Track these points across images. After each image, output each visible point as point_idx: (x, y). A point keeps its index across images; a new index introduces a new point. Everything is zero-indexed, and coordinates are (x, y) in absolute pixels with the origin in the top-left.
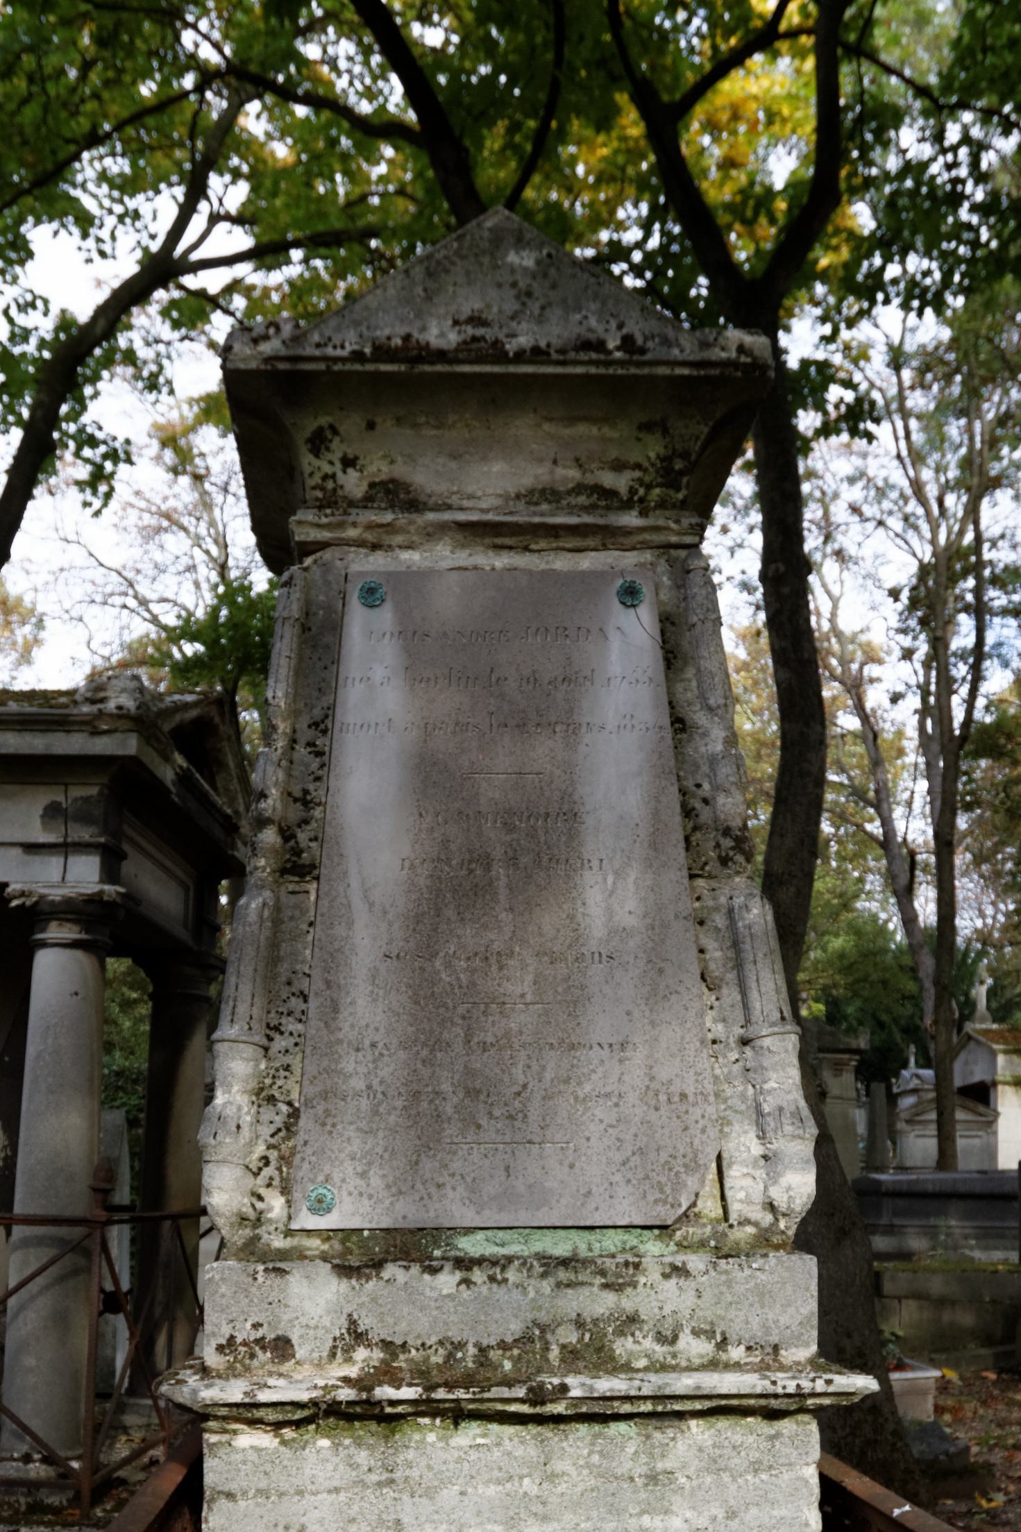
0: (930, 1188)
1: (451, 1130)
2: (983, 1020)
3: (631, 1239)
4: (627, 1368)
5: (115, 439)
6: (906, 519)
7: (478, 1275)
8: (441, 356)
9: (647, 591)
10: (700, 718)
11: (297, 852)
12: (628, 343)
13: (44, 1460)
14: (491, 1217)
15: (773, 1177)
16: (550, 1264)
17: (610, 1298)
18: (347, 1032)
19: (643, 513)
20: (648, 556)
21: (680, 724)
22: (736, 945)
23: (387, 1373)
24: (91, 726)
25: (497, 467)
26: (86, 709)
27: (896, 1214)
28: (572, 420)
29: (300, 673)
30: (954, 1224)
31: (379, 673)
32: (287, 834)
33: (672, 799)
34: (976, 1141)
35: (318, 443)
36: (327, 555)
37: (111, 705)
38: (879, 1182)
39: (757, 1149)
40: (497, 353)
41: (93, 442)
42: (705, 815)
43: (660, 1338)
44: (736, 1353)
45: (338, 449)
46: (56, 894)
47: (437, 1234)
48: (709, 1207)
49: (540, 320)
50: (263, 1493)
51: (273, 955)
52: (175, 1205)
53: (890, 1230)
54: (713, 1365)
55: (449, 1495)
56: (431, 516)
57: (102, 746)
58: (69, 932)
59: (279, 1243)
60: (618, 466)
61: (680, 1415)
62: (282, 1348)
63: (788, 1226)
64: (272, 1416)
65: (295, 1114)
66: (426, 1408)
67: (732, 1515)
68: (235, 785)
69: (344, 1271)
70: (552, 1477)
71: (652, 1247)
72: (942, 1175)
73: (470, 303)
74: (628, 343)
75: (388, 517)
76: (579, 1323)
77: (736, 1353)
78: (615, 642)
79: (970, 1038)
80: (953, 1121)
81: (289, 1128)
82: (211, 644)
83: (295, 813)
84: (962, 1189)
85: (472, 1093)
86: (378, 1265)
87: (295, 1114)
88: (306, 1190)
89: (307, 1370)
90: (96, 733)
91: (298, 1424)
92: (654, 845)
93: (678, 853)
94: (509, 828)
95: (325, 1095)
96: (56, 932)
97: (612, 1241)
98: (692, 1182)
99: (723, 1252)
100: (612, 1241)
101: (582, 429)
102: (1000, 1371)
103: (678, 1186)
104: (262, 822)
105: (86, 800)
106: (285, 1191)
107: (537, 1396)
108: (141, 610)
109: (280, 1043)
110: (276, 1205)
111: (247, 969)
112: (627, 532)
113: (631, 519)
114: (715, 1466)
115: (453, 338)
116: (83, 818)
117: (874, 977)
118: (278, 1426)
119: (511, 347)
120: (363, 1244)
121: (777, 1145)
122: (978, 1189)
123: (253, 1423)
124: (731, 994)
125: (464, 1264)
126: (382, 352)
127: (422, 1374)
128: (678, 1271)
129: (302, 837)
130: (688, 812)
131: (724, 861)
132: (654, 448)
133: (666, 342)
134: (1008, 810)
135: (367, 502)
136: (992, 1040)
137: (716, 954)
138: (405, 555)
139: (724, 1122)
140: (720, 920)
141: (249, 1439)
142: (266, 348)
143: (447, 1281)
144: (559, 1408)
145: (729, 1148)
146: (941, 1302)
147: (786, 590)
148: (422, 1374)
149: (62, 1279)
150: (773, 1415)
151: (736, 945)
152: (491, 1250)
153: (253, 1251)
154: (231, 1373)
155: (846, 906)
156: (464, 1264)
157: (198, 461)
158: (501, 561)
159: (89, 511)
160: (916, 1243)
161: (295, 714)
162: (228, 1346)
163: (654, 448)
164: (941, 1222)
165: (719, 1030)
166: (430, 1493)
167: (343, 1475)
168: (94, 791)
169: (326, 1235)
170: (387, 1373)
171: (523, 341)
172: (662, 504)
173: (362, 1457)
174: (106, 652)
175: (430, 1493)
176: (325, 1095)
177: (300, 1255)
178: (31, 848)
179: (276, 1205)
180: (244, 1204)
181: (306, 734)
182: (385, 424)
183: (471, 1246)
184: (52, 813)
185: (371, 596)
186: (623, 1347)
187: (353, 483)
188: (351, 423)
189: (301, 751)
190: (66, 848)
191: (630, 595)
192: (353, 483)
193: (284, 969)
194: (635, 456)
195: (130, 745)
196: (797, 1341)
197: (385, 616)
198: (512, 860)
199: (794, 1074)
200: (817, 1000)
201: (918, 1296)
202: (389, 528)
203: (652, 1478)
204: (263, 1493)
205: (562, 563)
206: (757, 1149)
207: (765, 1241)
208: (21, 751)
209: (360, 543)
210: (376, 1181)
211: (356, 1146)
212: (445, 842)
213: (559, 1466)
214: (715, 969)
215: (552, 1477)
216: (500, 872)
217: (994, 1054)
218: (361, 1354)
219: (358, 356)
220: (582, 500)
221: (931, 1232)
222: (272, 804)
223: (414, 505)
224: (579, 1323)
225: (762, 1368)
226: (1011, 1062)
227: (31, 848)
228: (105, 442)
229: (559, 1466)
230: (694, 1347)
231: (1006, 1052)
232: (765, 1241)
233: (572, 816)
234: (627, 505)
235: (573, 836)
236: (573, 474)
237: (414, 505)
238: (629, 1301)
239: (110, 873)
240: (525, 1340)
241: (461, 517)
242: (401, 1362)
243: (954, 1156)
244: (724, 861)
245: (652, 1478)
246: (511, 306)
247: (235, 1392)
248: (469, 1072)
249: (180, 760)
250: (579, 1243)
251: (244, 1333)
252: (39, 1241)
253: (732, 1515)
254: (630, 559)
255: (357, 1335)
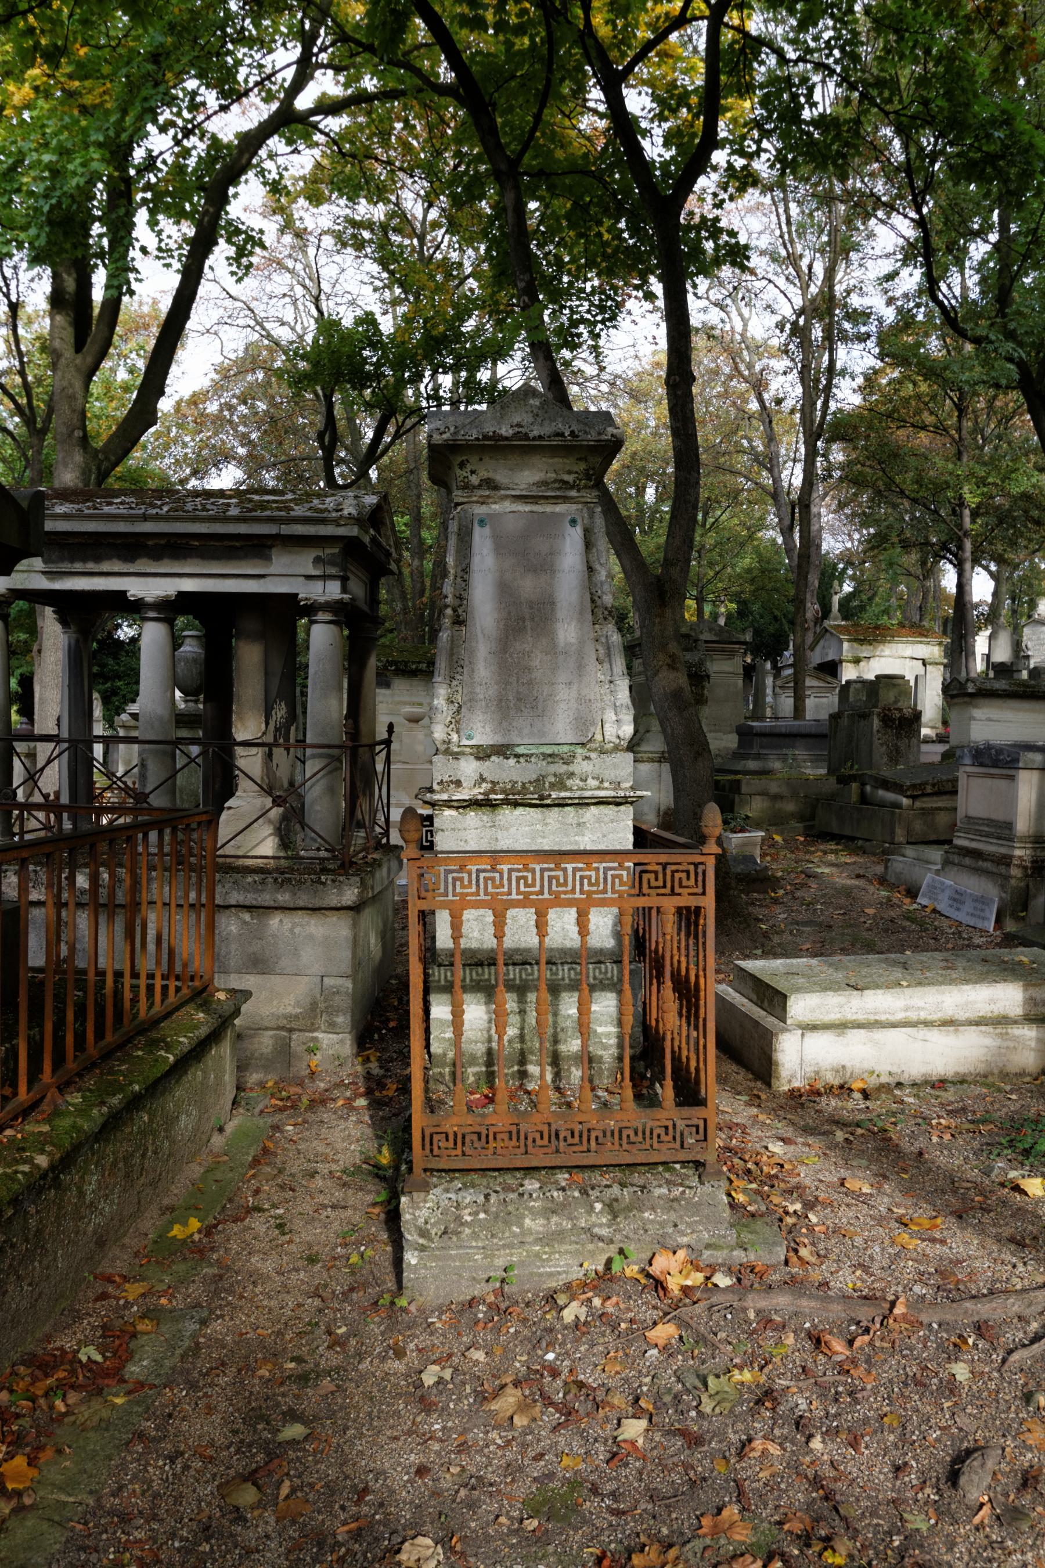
0: (783, 730)
1: (512, 712)
2: (835, 619)
3: (572, 748)
4: (571, 789)
5: (253, 230)
6: (787, 279)
7: (522, 760)
8: (507, 439)
9: (579, 521)
10: (597, 567)
11: (458, 616)
12: (572, 433)
13: (326, 850)
14: (526, 741)
15: (619, 728)
16: (545, 756)
17: (565, 767)
18: (477, 679)
19: (578, 491)
20: (580, 506)
21: (590, 569)
22: (608, 648)
23: (493, 791)
24: (336, 522)
25: (526, 473)
26: (334, 514)
27: (762, 747)
28: (553, 457)
29: (458, 551)
30: (800, 753)
31: (485, 551)
32: (455, 610)
33: (588, 596)
34: (825, 700)
35: (462, 466)
36: (465, 506)
37: (346, 512)
38: (752, 727)
39: (614, 718)
40: (526, 437)
41: (238, 232)
42: (599, 602)
43: (581, 780)
44: (606, 785)
45: (469, 467)
46: (322, 599)
47: (509, 746)
48: (598, 737)
49: (541, 425)
50: (453, 829)
51: (452, 653)
52: (365, 741)
53: (758, 757)
54: (599, 788)
55: (513, 830)
56: (503, 492)
57: (341, 531)
58: (328, 617)
59: (456, 749)
60: (570, 472)
61: (588, 804)
62: (458, 783)
63: (625, 744)
64: (456, 804)
65: (460, 707)
66: (506, 802)
67: (604, 836)
68: (389, 533)
69: (478, 758)
70: (546, 824)
71: (579, 751)
72: (797, 723)
73: (517, 419)
74: (572, 433)
75: (487, 493)
76: (555, 775)
77: (606, 785)
78: (568, 541)
79: (827, 631)
80: (804, 688)
81: (458, 711)
82: (316, 364)
83: (457, 602)
84: (803, 731)
85: (519, 700)
86: (489, 756)
87: (460, 707)
88: (465, 732)
89: (466, 791)
90: (338, 525)
91: (464, 807)
92: (581, 613)
93: (589, 616)
94: (531, 608)
95: (470, 700)
96: (321, 616)
97: (566, 749)
98: (592, 729)
99: (602, 751)
100: (566, 749)
101: (556, 460)
102: (806, 836)
103: (588, 730)
104: (446, 606)
105: (333, 554)
106: (458, 732)
107: (542, 798)
108: (258, 328)
109: (455, 683)
110: (455, 737)
111: (443, 658)
112: (572, 498)
113: (573, 493)
114: (599, 821)
115: (511, 432)
116: (332, 564)
117: (770, 586)
118: (457, 808)
119: (531, 435)
120: (484, 750)
121: (621, 716)
122: (813, 731)
123: (449, 807)
124: (606, 666)
125: (517, 756)
126: (486, 437)
127: (503, 791)
128: (588, 758)
129: (460, 611)
130: (593, 601)
131: (605, 619)
132: (582, 466)
133: (586, 433)
134: (853, 478)
135: (480, 486)
136: (841, 633)
137: (602, 651)
138: (494, 506)
139: (603, 709)
140: (603, 640)
141: (448, 813)
142: (445, 436)
143: (512, 761)
144: (548, 802)
145: (605, 718)
146: (776, 797)
147: (679, 393)
148: (503, 791)
149: (330, 772)
150: (618, 804)
151: (608, 648)
152: (526, 752)
153: (447, 752)
154: (442, 791)
155: (751, 537)
156: (517, 756)
157: (298, 223)
158: (528, 508)
159: (235, 278)
160: (777, 765)
161: (456, 566)
162: (441, 783)
163: (582, 466)
164: (790, 752)
165: (602, 678)
166: (507, 829)
167: (479, 824)
168: (337, 550)
169: (472, 747)
170: (493, 791)
171: (536, 433)
172: (586, 487)
173: (485, 818)
174: (233, 356)
175: (507, 829)
176: (470, 700)
177: (463, 753)
178: (309, 577)
179: (455, 737)
180: (445, 737)
181: (461, 574)
182: (486, 459)
183: (520, 750)
184: (317, 560)
185: (482, 523)
186: (569, 783)
187: (474, 480)
188: (474, 459)
189: (459, 580)
190: (324, 577)
191: (573, 522)
192: (474, 480)
193: (455, 658)
194: (576, 468)
195: (354, 531)
196: (626, 780)
197: (487, 530)
198: (532, 619)
199: (627, 693)
200: (731, 602)
201: (763, 793)
202: (488, 497)
203: (579, 825)
204: (453, 829)
205: (549, 508)
206: (614, 718)
207: (616, 748)
208: (72, 340)
209: (477, 502)
210: (488, 729)
211: (481, 717)
212: (509, 613)
213: (548, 821)
214: (601, 657)
215: (546, 824)
216: (528, 623)
217: (841, 642)
218: (484, 785)
219: (477, 439)
220: (557, 485)
221: (784, 758)
222: (449, 600)
223: (496, 488)
224: (555, 775)
225: (614, 789)
226: (852, 647)
227: (309, 577)
228: (246, 232)
229: (548, 821)
230: (592, 783)
231: (849, 641)
232: (616, 748)
233: (553, 603)
234: (572, 487)
235: (553, 610)
236: (554, 475)
237: (496, 488)
238: (571, 768)
239: (344, 590)
240: (537, 780)
241: (513, 493)
242: (497, 788)
243: (804, 710)
244: (605, 619)
245: (579, 825)
246: (531, 420)
247: (445, 797)
248: (518, 693)
249: (372, 532)
250: (555, 749)
251: (446, 778)
252: (320, 756)
253: (604, 836)
254: (574, 507)
255: (483, 779)
